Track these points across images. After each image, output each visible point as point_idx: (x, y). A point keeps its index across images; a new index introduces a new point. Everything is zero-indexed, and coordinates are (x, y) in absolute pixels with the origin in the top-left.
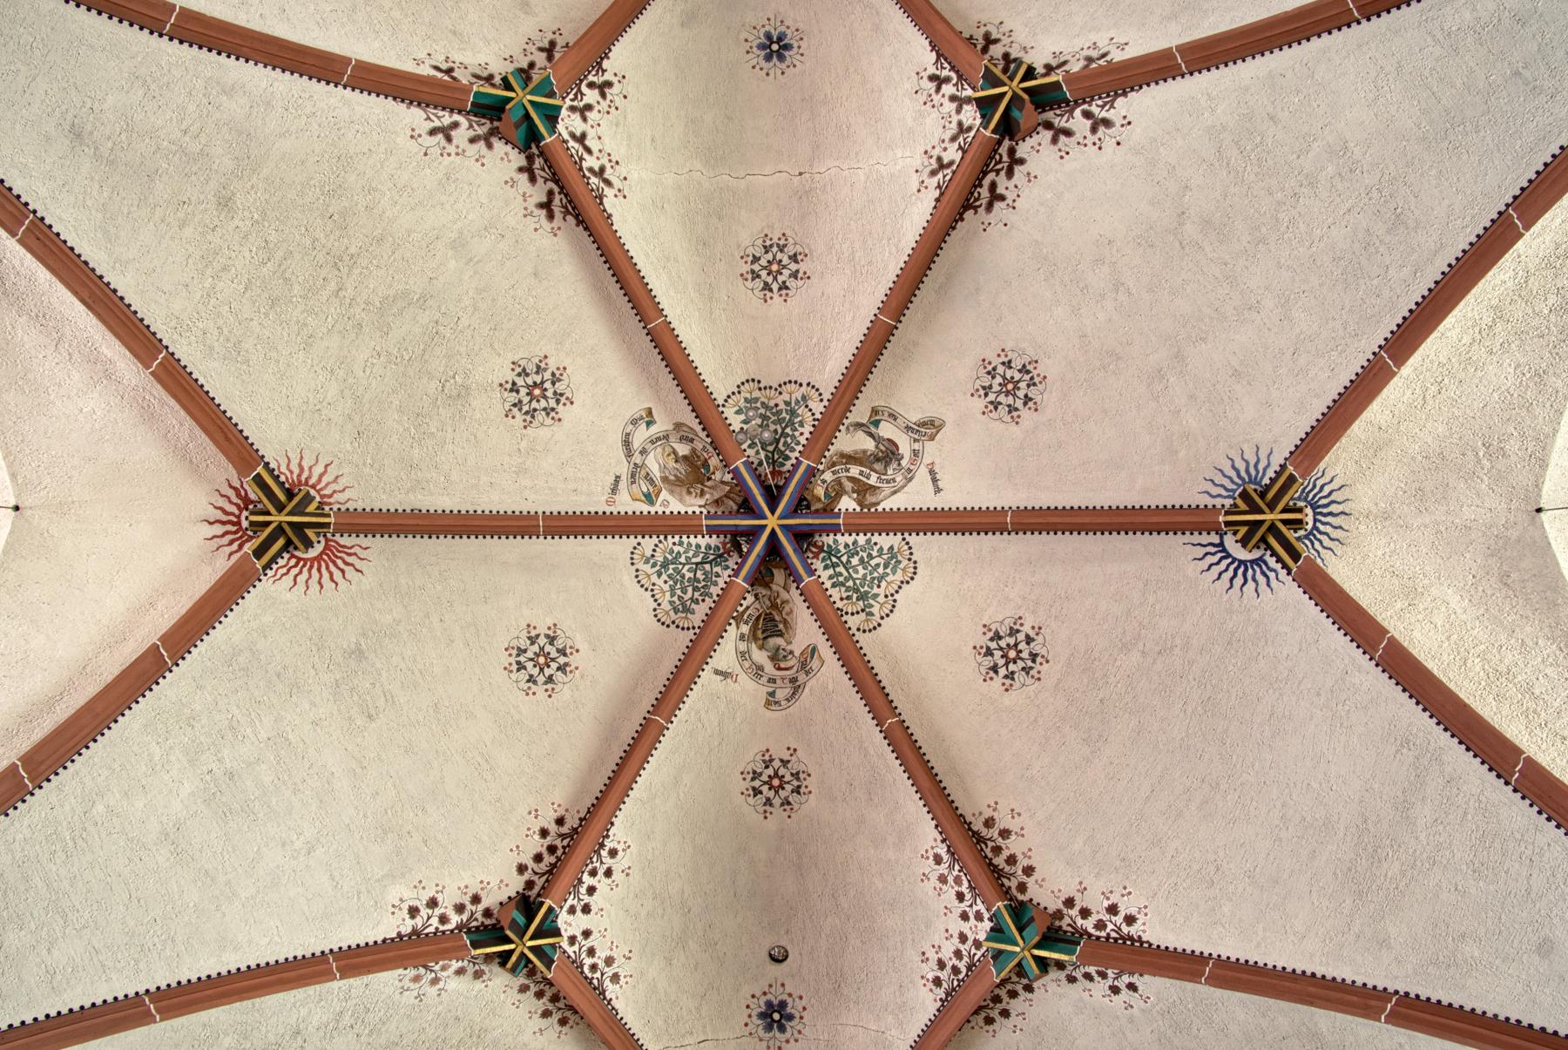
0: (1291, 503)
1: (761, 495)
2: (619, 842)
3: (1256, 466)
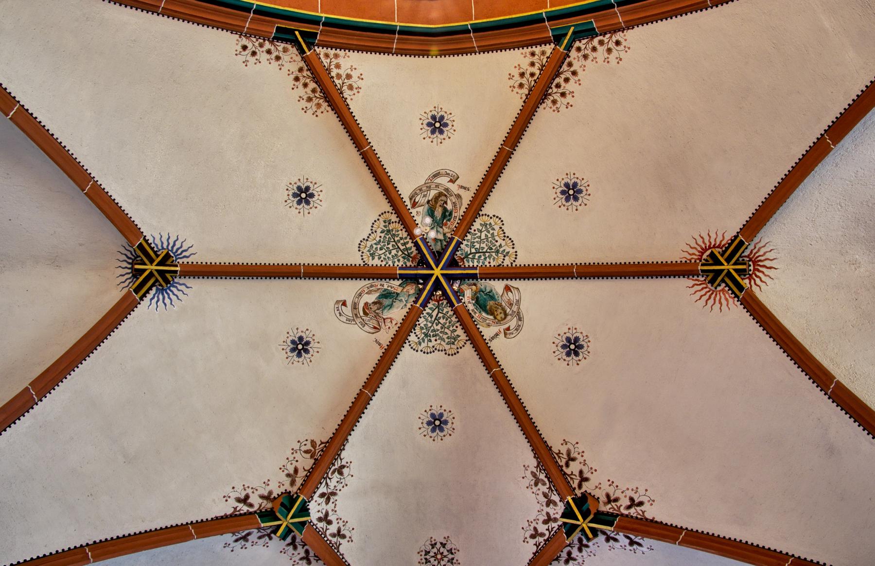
0: (741, 259)
3: (158, 301)
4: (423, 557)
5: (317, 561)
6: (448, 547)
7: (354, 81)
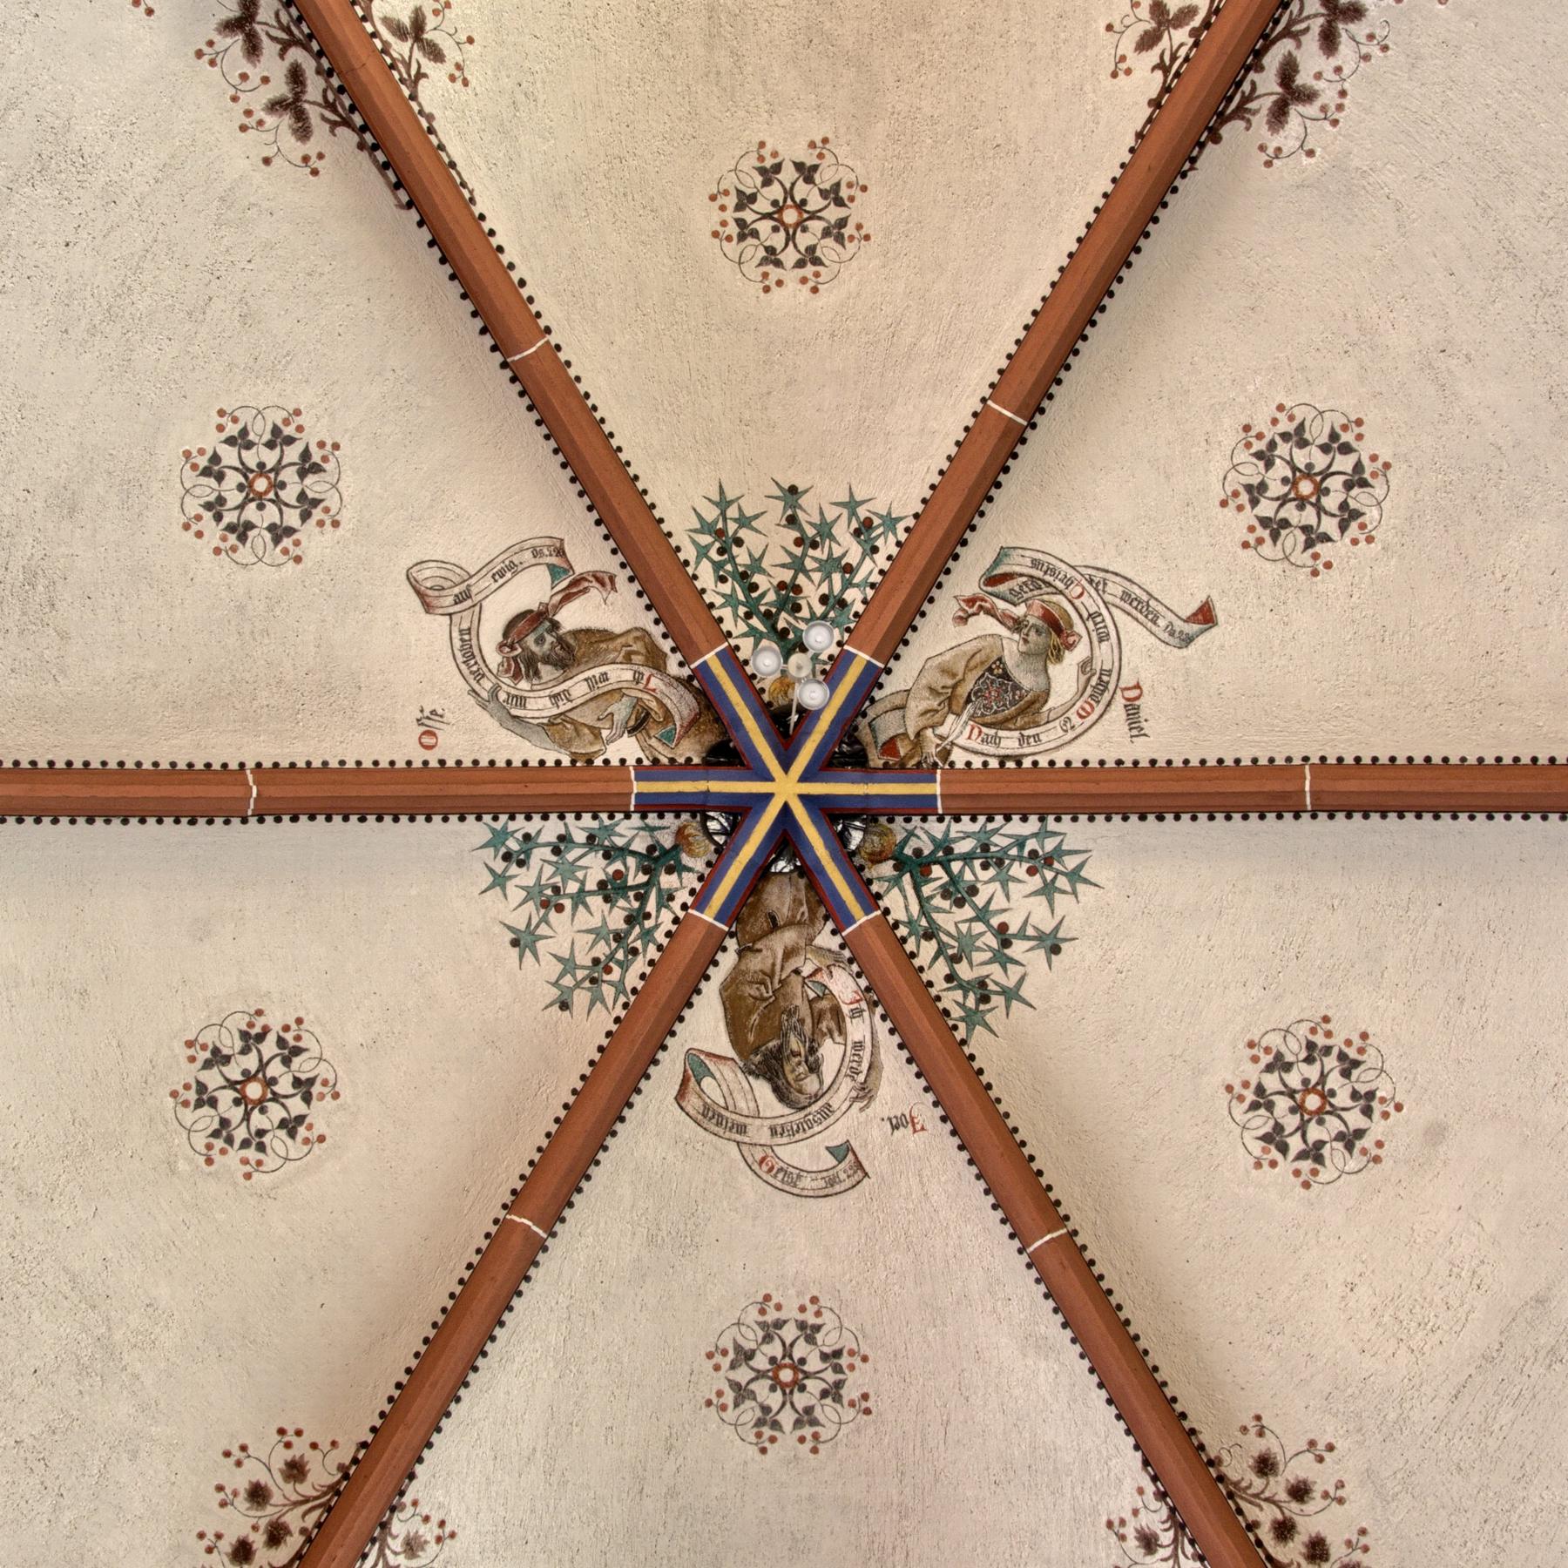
1: (766, 734)
2: (426, 1519)
4: (729, 215)
5: (334, 125)
6: (825, 178)
7: (265, 1467)
